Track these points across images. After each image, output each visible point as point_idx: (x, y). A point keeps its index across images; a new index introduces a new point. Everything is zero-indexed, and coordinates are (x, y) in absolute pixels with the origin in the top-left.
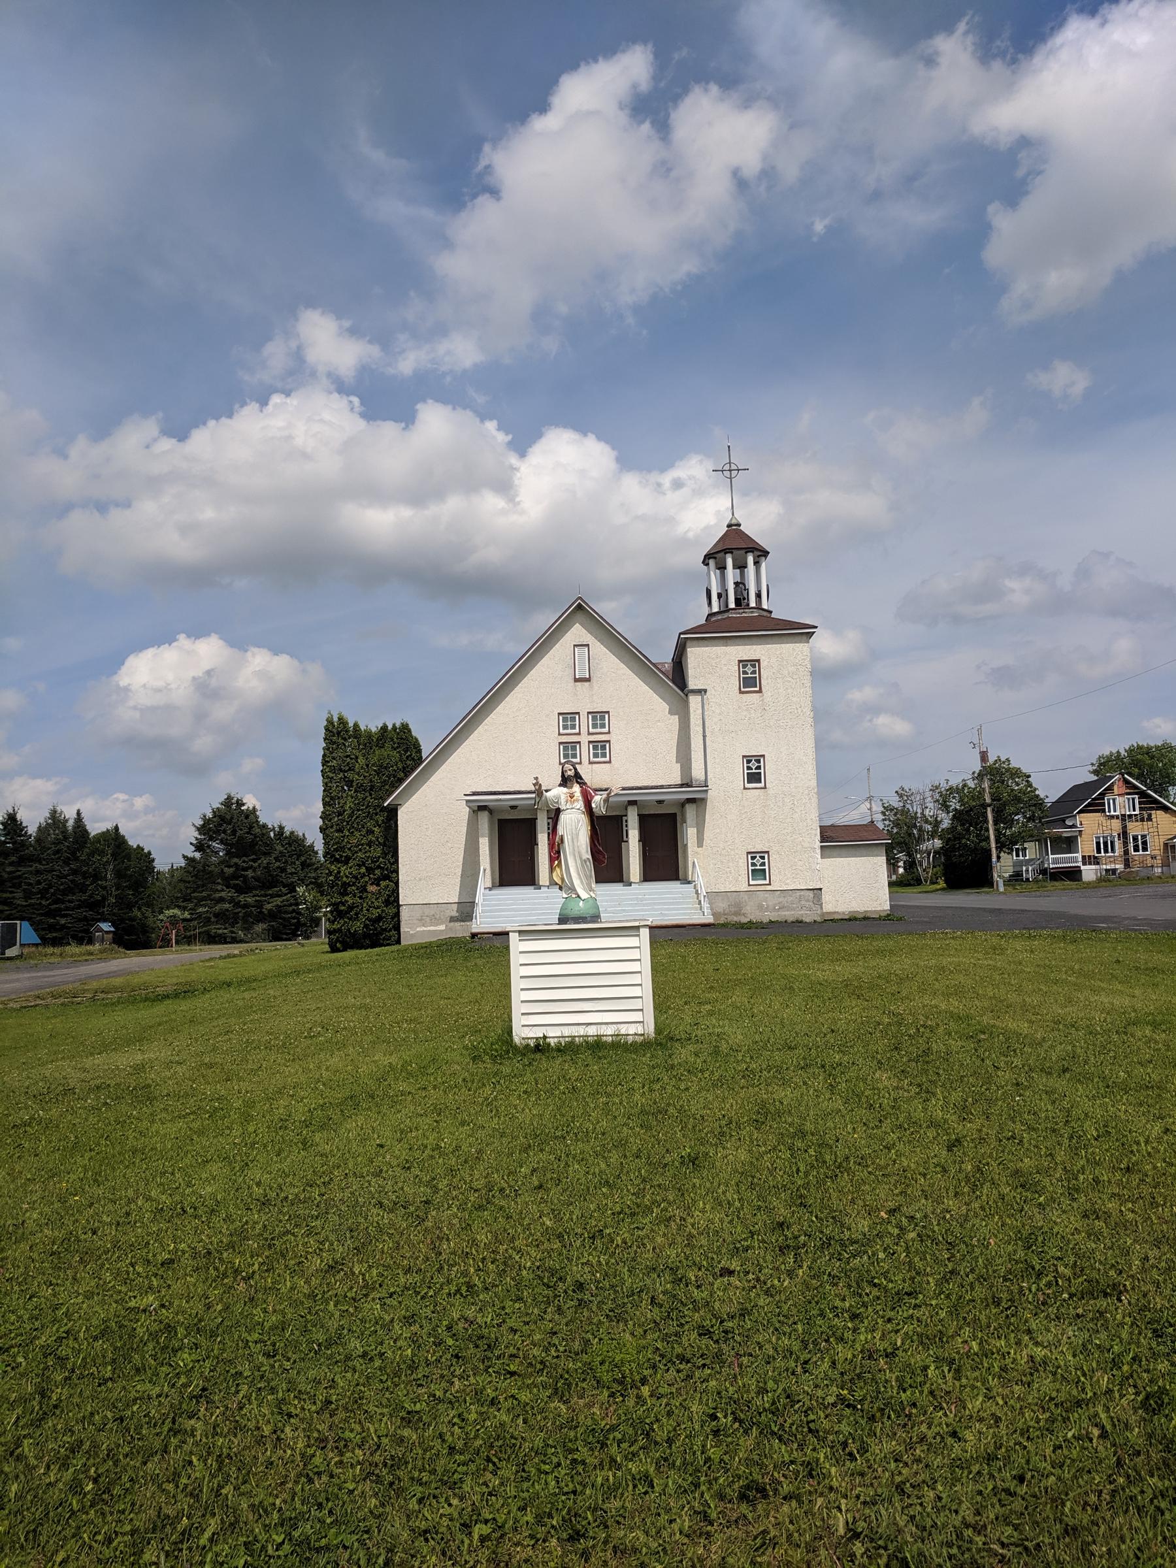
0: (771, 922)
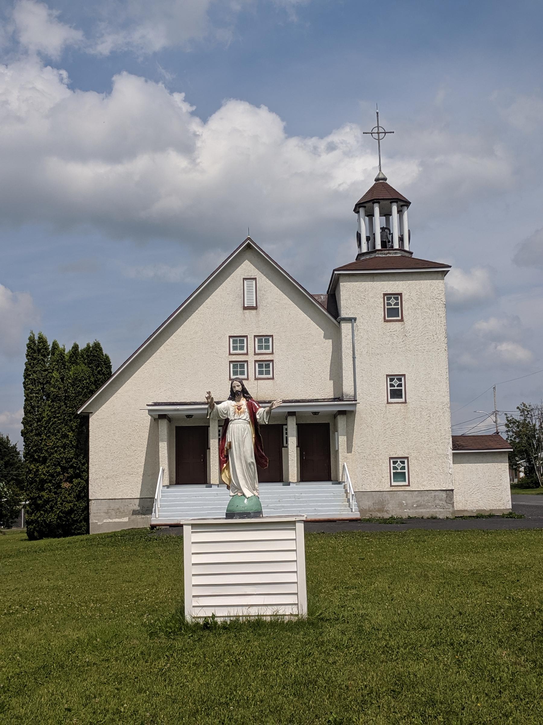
0: (409, 518)
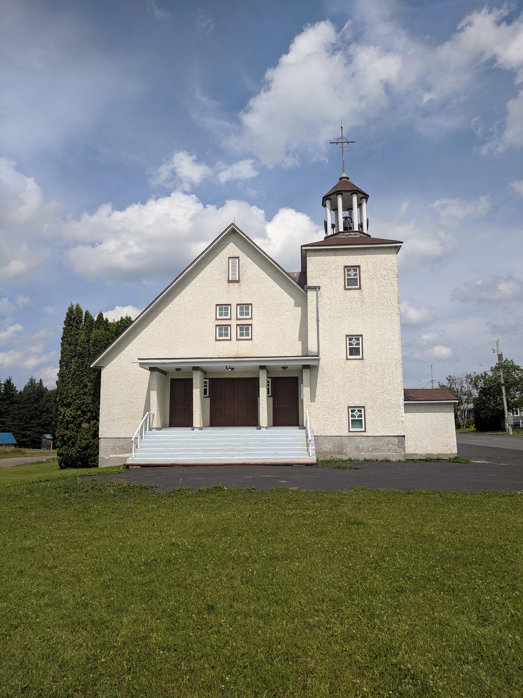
0: (366, 460)
